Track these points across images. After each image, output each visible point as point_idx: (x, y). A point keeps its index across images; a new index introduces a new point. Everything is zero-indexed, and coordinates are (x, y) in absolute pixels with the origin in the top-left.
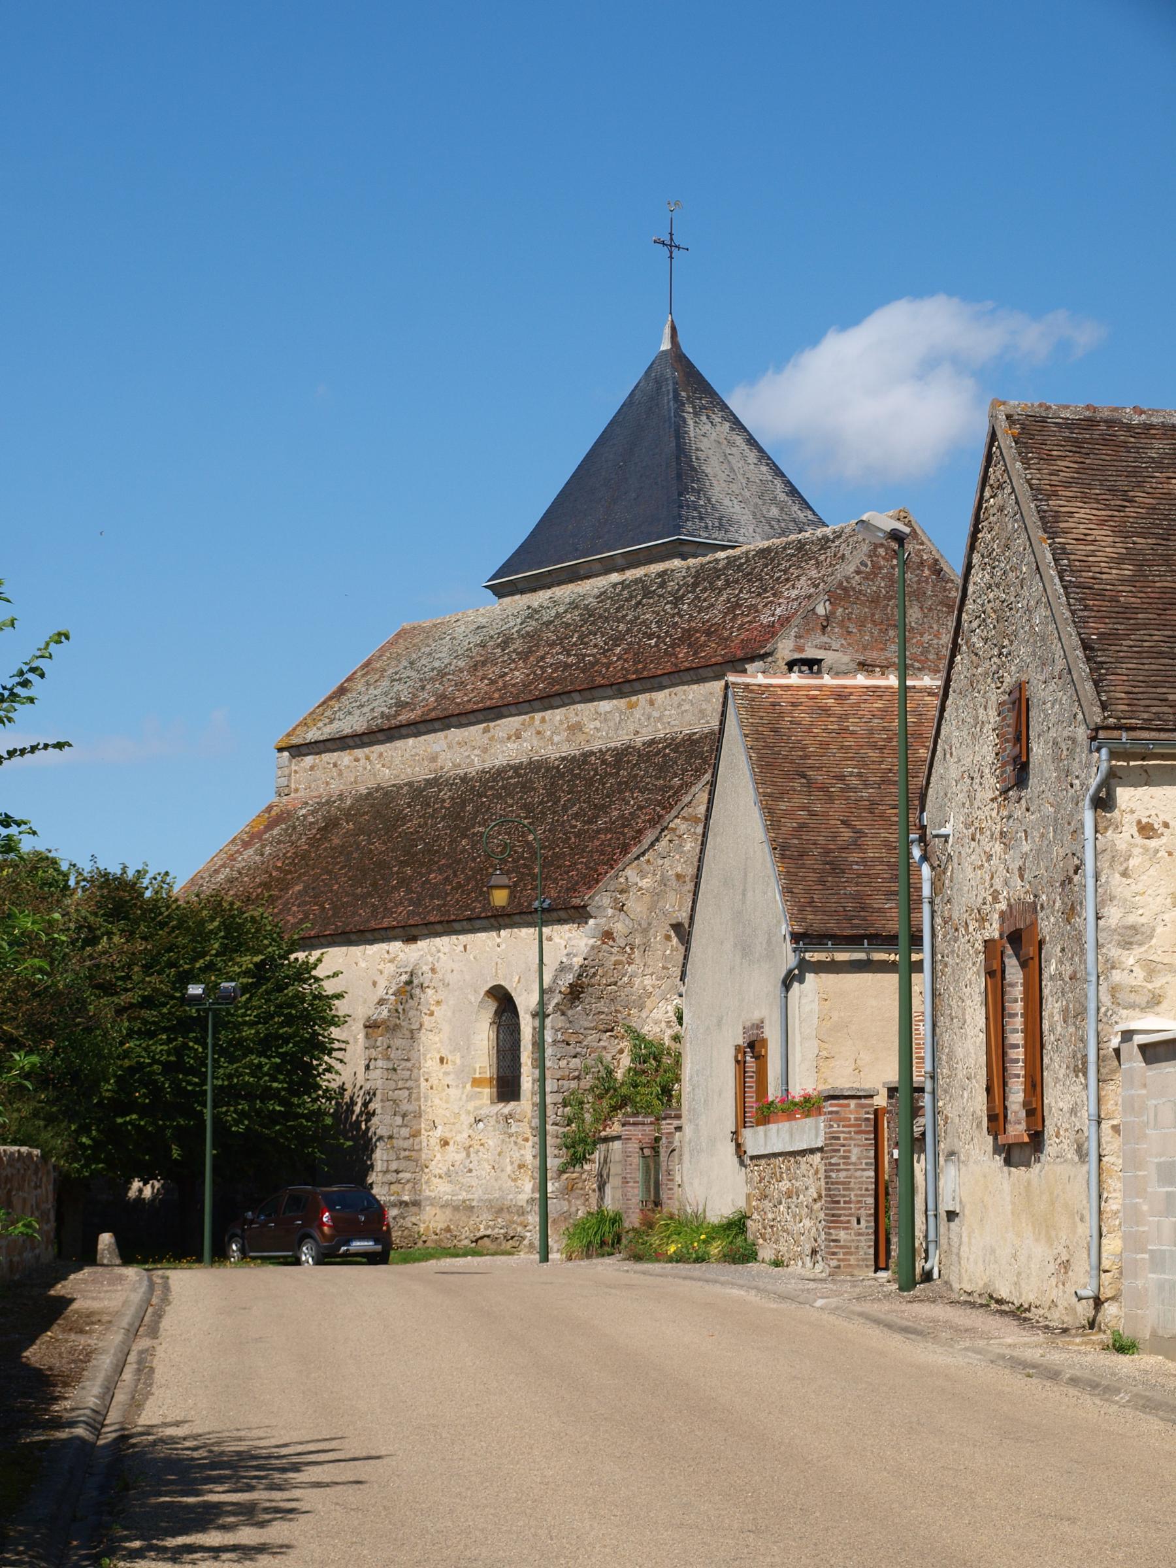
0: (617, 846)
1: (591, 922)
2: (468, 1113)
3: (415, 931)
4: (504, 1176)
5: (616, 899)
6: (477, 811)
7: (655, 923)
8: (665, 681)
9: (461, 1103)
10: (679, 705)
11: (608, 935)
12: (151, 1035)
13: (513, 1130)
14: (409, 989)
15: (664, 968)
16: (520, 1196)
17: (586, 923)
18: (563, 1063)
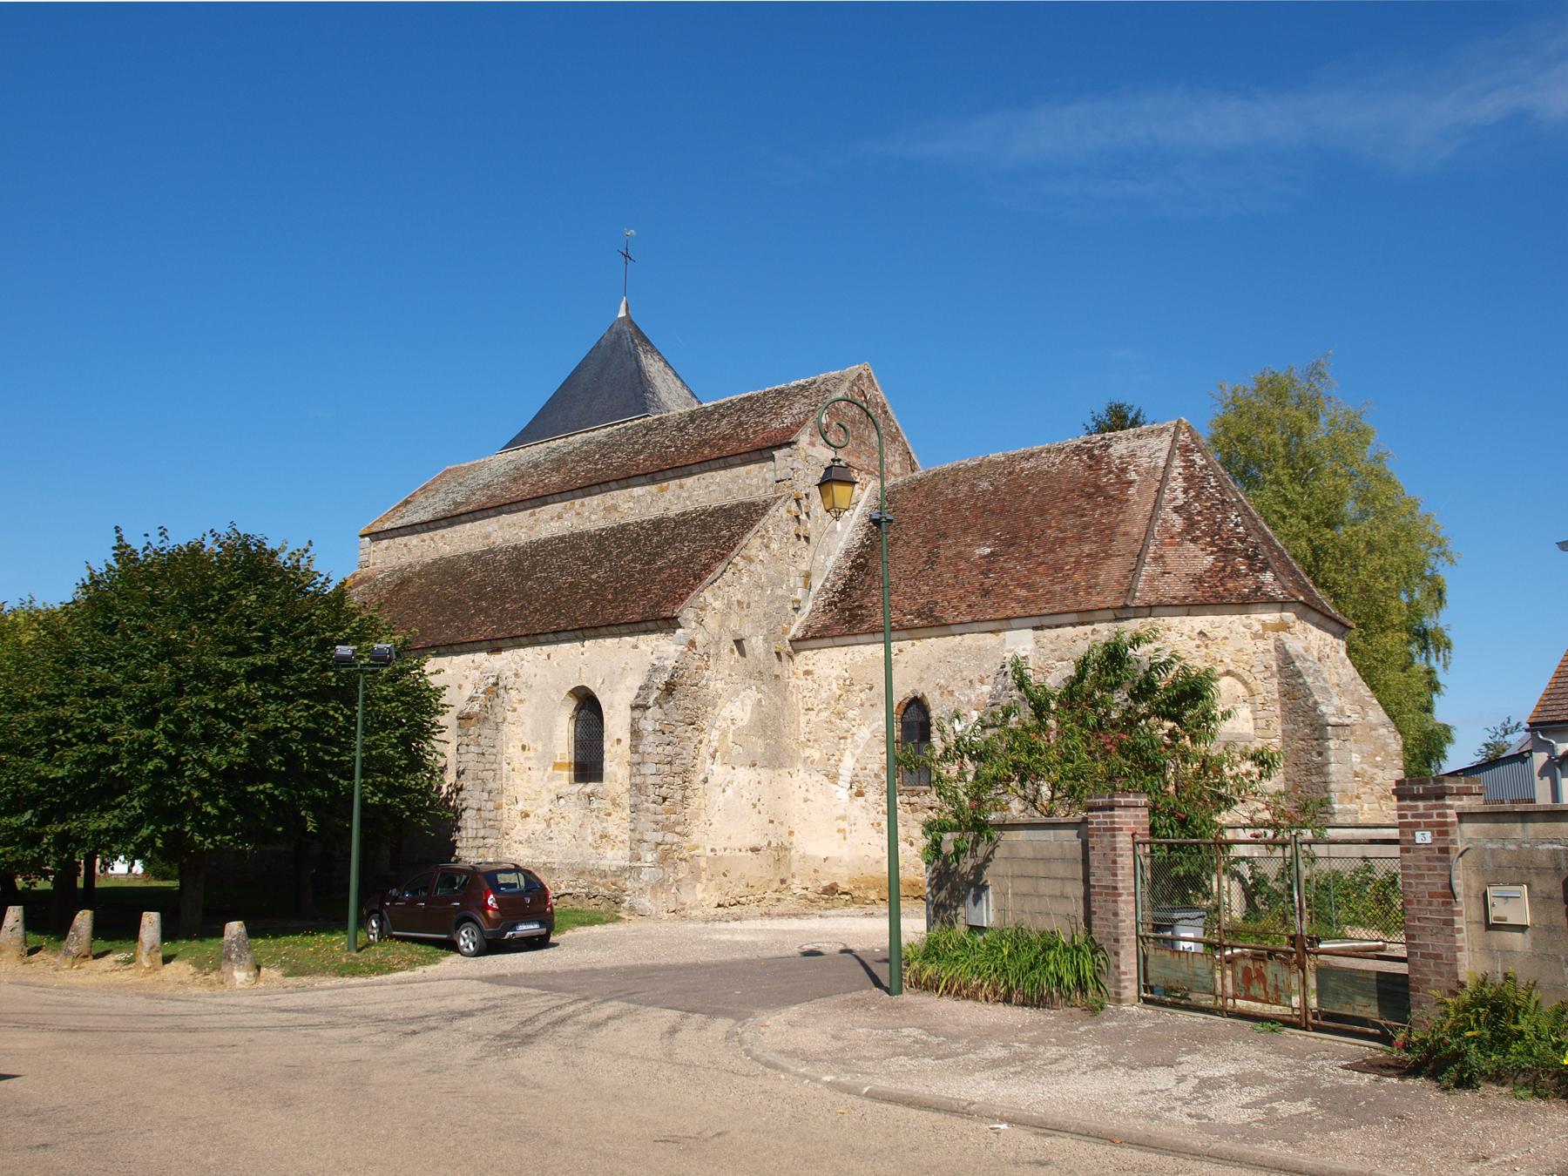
0: (691, 576)
1: (679, 631)
3: (500, 644)
4: (585, 844)
6: (534, 566)
8: (695, 468)
11: (692, 643)
12: (289, 699)
13: (595, 805)
14: (495, 689)
18: (660, 749)
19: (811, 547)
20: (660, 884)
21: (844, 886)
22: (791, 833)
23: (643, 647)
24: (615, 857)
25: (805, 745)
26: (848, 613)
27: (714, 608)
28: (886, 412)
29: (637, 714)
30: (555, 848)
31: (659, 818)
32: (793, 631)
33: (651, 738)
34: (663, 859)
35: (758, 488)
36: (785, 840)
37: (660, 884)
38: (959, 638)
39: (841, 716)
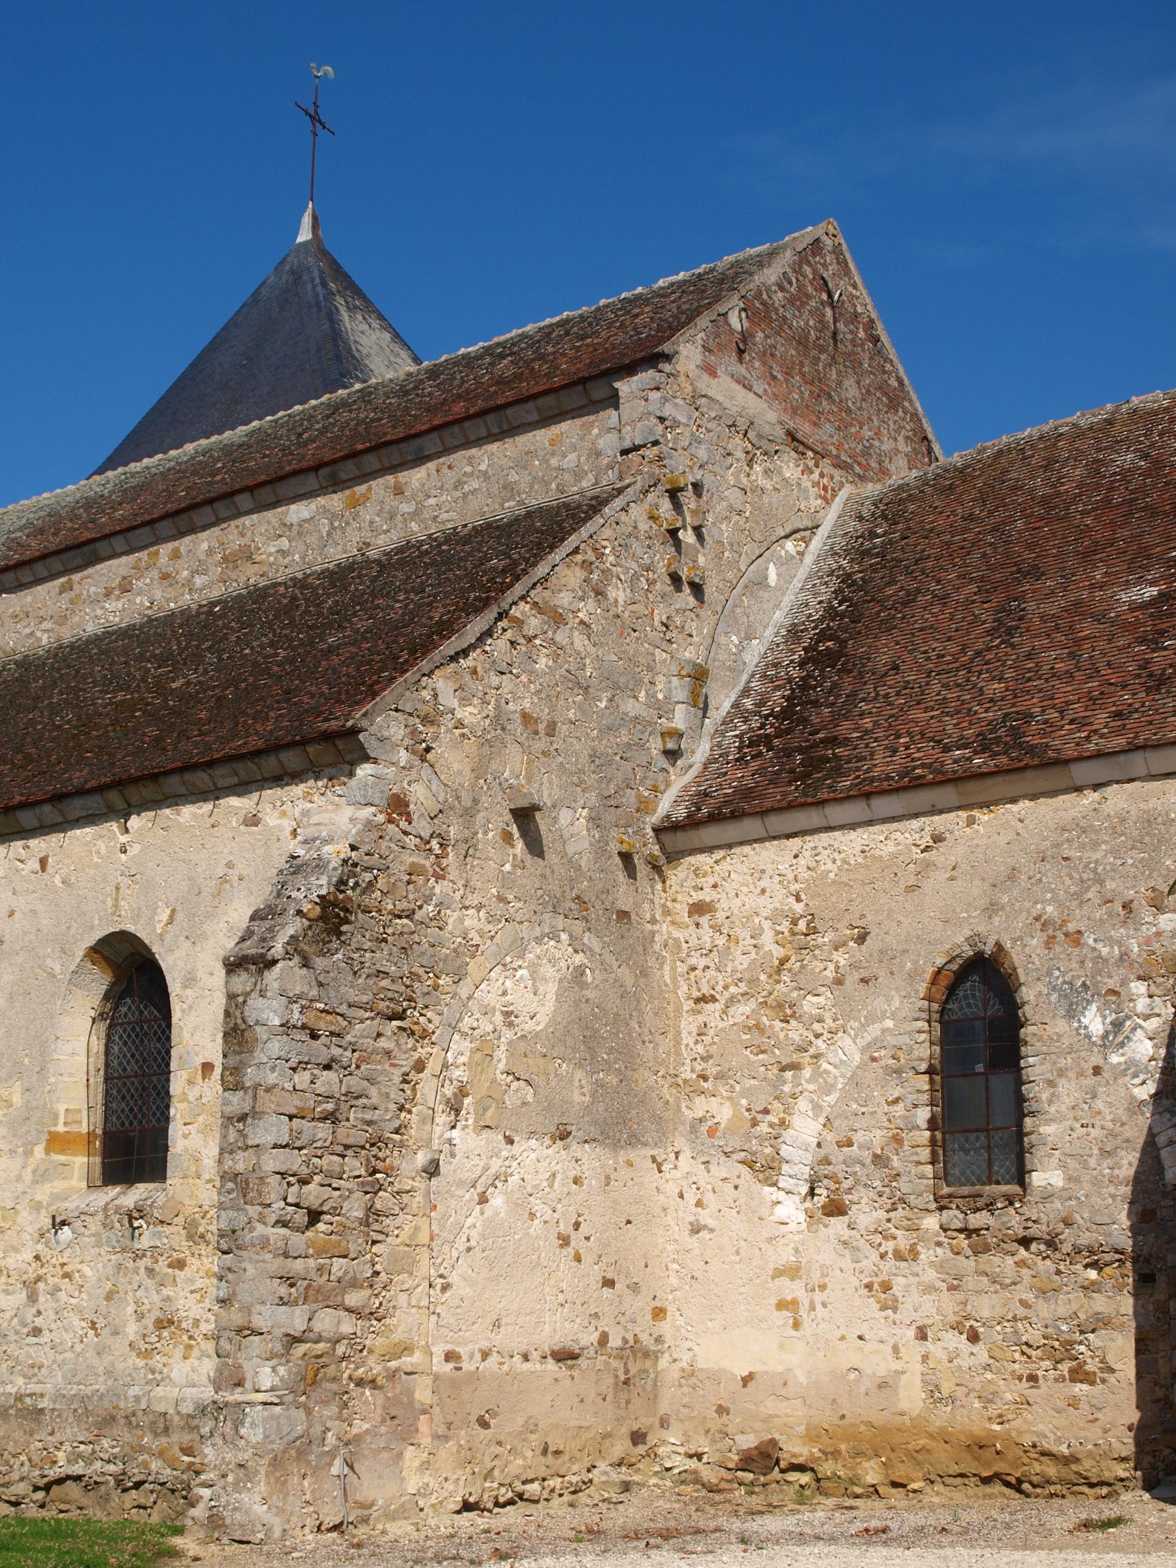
1: (364, 771)
2: (37, 1207)
4: (120, 1345)
5: (414, 732)
7: (485, 801)
8: (431, 443)
9: (20, 1187)
10: (458, 484)
11: (398, 806)
13: (145, 1242)
15: (501, 899)
16: (159, 1391)
17: (351, 774)
19: (705, 612)
20: (295, 1455)
21: (795, 1449)
22: (659, 1313)
23: (271, 819)
24: (188, 1377)
25: (693, 1090)
26: (803, 755)
27: (458, 727)
28: (876, 340)
29: (242, 982)
30: (45, 1357)
31: (298, 1265)
32: (664, 805)
33: (275, 1047)
34: (309, 1382)
35: (578, 474)
36: (644, 1330)
37: (295, 1455)
38: (1092, 797)
39: (786, 1012)
